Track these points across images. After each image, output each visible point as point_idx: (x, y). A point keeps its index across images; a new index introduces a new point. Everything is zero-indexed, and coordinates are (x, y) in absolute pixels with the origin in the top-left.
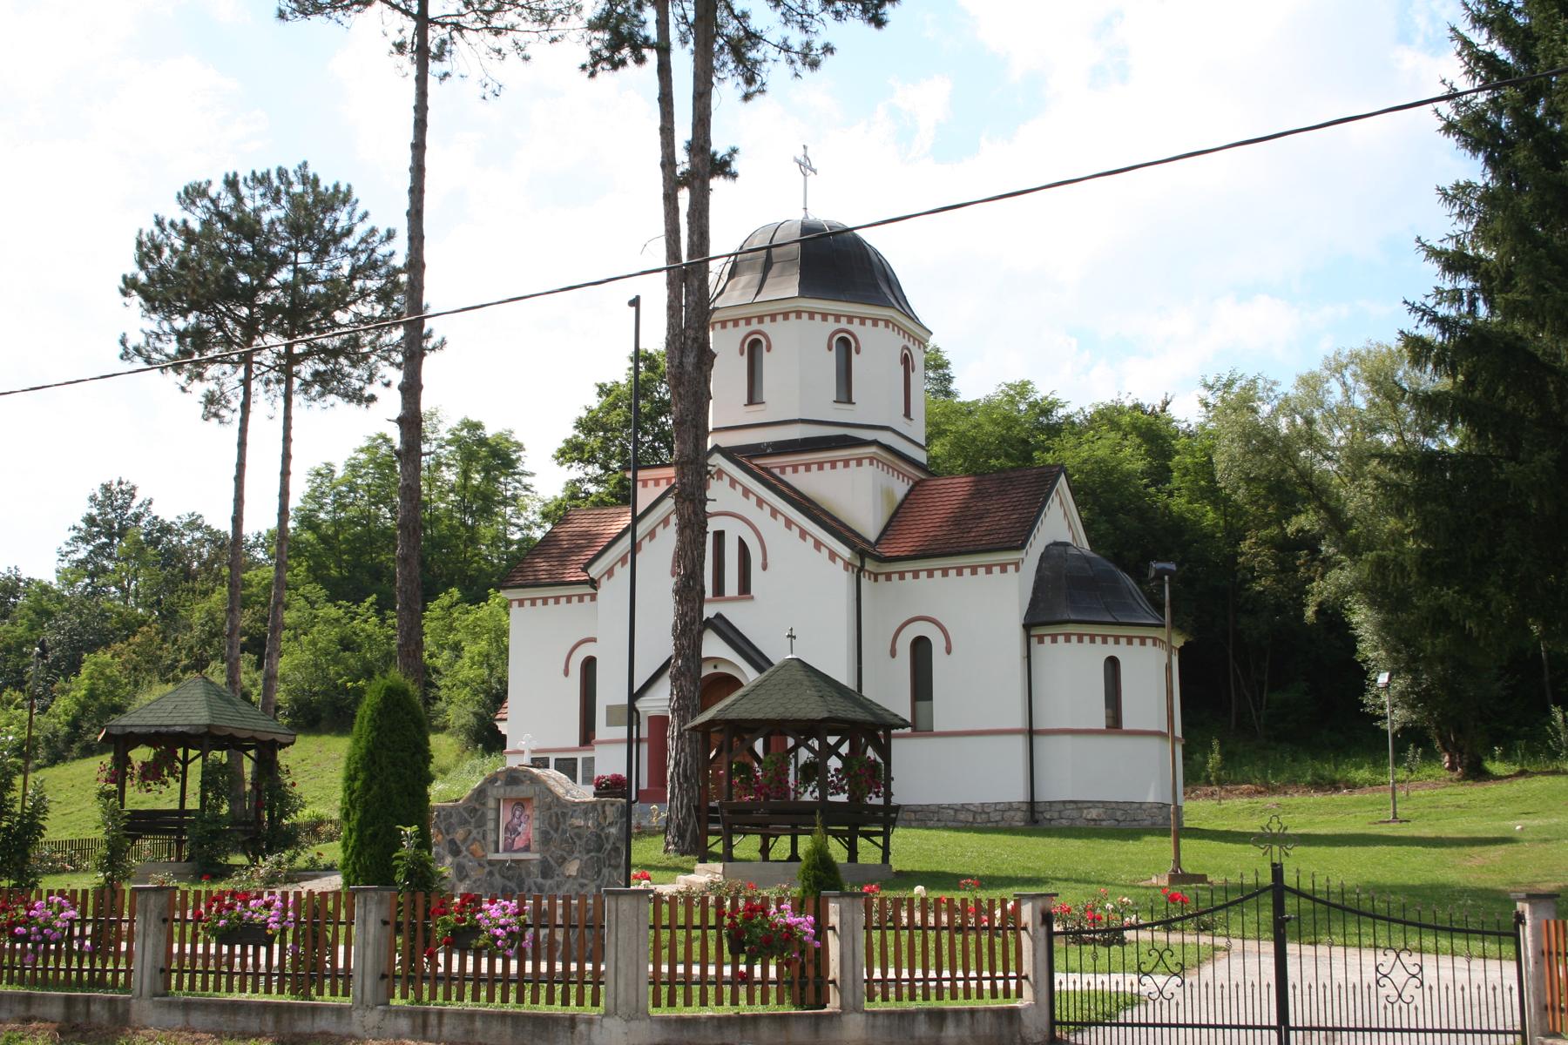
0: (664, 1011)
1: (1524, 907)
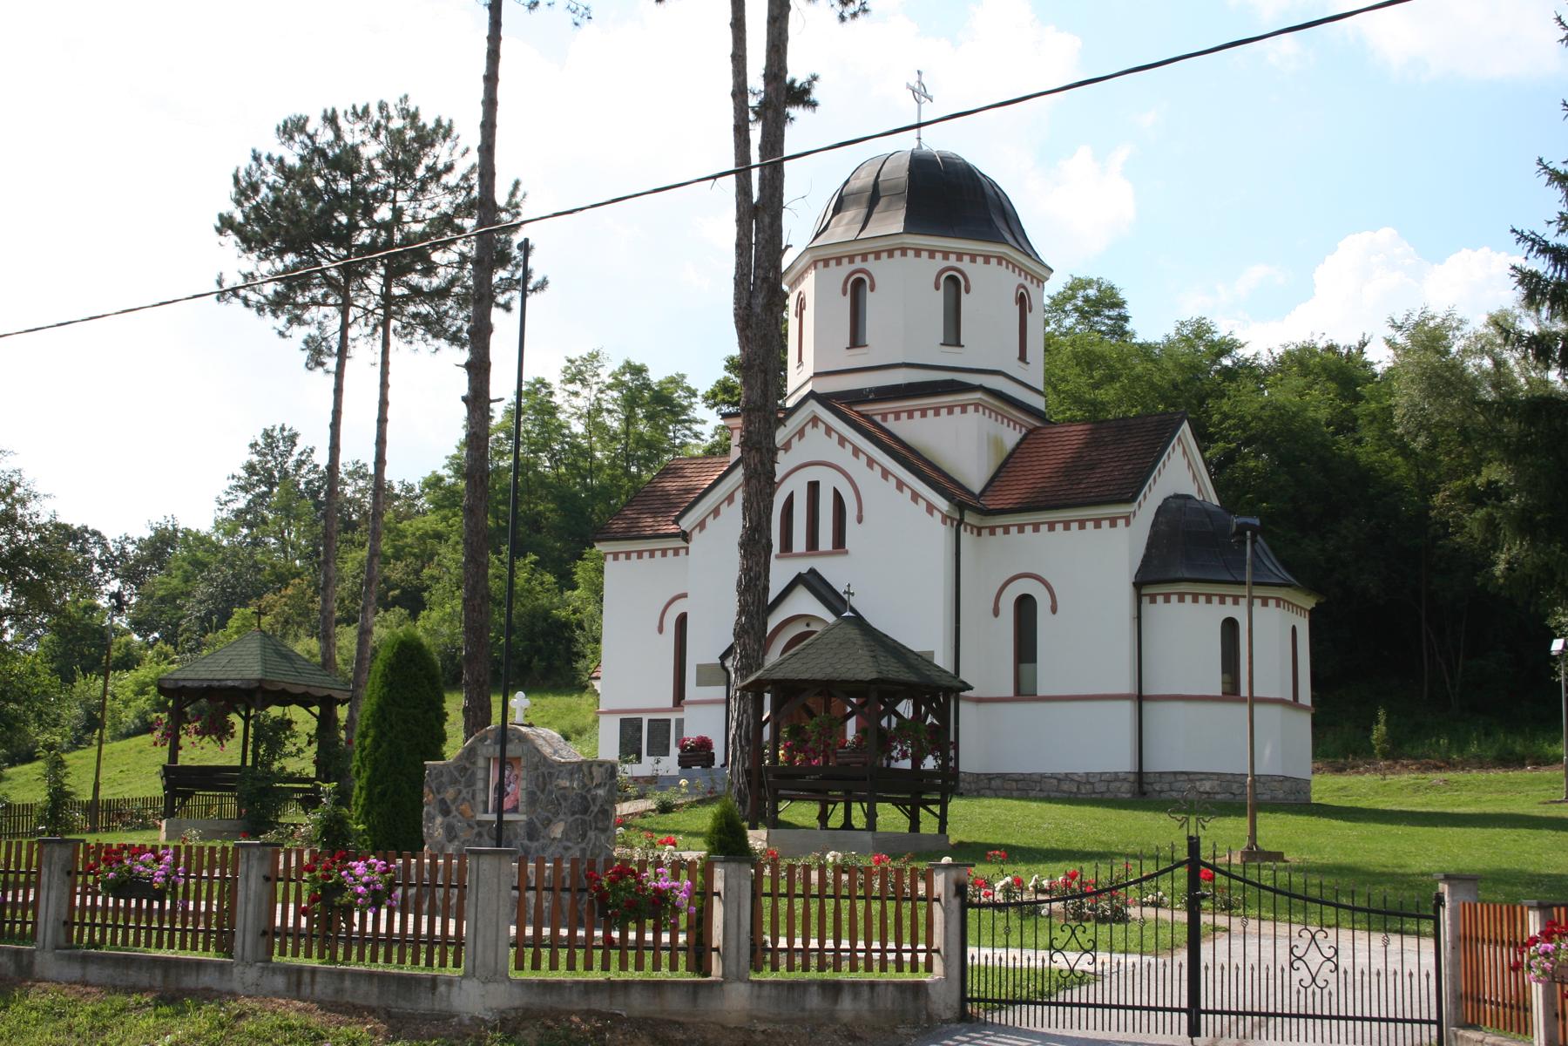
0: (528, 975)
1: (1444, 888)
